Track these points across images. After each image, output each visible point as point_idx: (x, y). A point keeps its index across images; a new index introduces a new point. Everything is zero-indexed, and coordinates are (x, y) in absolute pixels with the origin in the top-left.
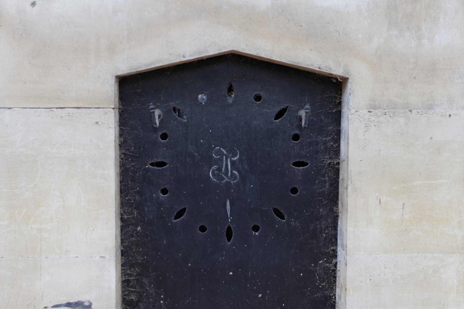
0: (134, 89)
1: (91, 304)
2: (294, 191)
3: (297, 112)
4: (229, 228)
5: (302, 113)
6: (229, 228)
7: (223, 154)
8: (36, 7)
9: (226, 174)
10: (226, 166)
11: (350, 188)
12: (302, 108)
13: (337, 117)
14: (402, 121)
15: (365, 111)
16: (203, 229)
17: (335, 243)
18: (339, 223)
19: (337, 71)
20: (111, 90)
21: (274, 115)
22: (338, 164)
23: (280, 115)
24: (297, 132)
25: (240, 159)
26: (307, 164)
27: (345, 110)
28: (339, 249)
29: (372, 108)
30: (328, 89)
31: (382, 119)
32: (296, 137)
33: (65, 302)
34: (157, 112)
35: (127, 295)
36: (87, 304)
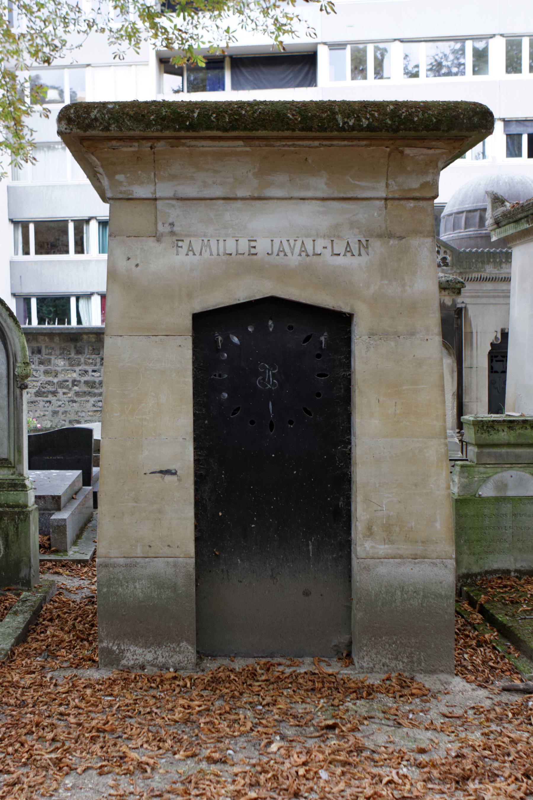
0: (205, 324)
1: (176, 472)
2: (319, 395)
3: (319, 338)
4: (271, 422)
5: (323, 339)
6: (271, 422)
7: (266, 368)
8: (139, 268)
9: (269, 383)
10: (269, 378)
11: (357, 391)
12: (322, 335)
13: (348, 342)
14: (393, 344)
15: (367, 337)
16: (252, 422)
17: (349, 433)
18: (211, 308)
19: (346, 309)
20: (188, 323)
21: (302, 340)
22: (350, 375)
23: (306, 340)
24: (319, 352)
25: (278, 372)
26: (327, 375)
27: (353, 336)
28: (352, 437)
29: (371, 334)
30: (340, 323)
31: (378, 342)
32: (319, 356)
33: (158, 470)
34: (220, 338)
35: (198, 470)
36: (174, 471)
